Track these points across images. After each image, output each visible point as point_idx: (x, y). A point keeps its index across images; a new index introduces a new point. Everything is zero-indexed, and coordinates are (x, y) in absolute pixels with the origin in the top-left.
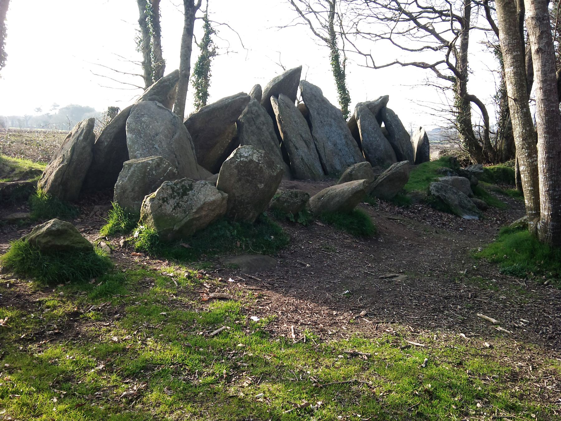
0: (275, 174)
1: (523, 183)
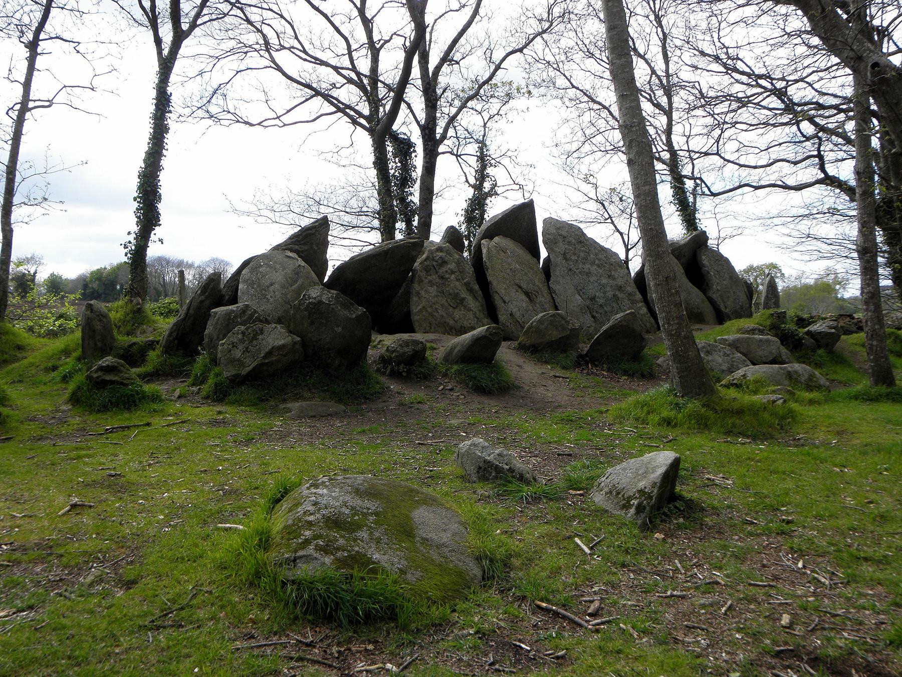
0: (354, 316)
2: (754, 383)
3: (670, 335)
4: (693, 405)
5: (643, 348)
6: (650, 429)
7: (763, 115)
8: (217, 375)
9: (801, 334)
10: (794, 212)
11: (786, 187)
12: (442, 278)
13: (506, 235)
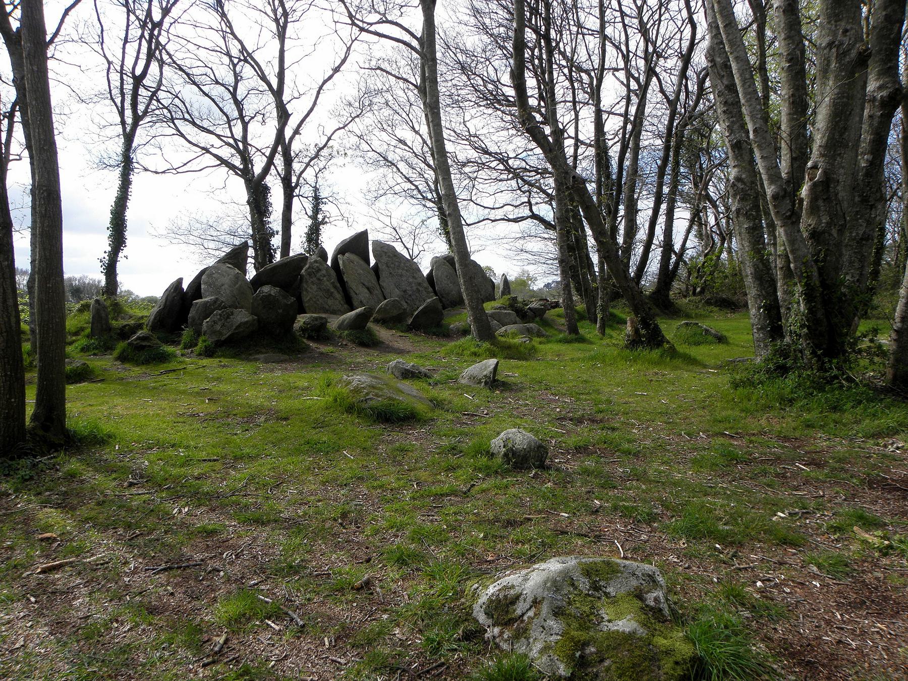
1: (36, 380)
2: (511, 333)
3: (472, 308)
4: (486, 345)
5: (442, 319)
6: (466, 358)
7: (495, 175)
8: (204, 341)
9: (527, 311)
10: (513, 235)
11: (509, 220)
12: (319, 279)
13: (352, 252)
